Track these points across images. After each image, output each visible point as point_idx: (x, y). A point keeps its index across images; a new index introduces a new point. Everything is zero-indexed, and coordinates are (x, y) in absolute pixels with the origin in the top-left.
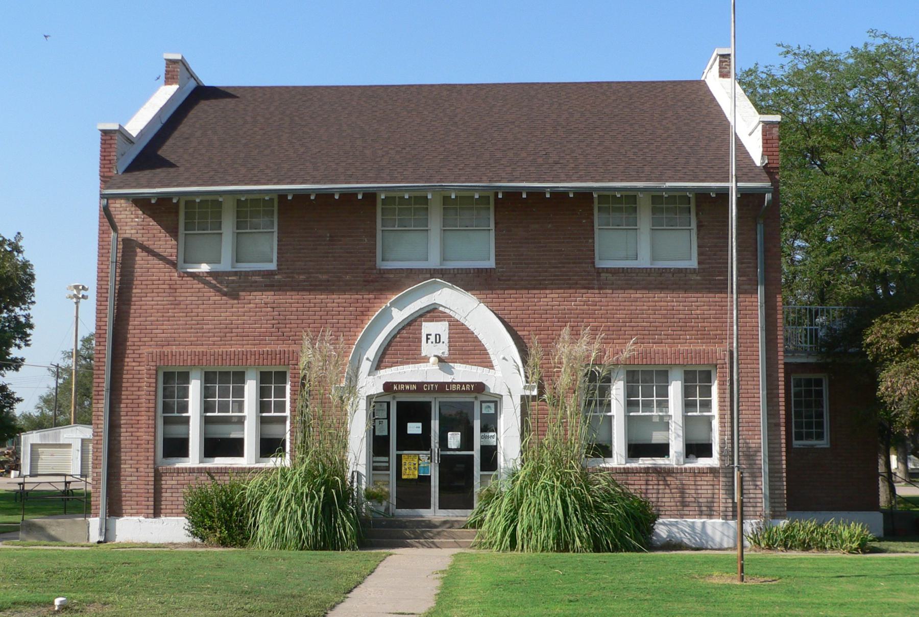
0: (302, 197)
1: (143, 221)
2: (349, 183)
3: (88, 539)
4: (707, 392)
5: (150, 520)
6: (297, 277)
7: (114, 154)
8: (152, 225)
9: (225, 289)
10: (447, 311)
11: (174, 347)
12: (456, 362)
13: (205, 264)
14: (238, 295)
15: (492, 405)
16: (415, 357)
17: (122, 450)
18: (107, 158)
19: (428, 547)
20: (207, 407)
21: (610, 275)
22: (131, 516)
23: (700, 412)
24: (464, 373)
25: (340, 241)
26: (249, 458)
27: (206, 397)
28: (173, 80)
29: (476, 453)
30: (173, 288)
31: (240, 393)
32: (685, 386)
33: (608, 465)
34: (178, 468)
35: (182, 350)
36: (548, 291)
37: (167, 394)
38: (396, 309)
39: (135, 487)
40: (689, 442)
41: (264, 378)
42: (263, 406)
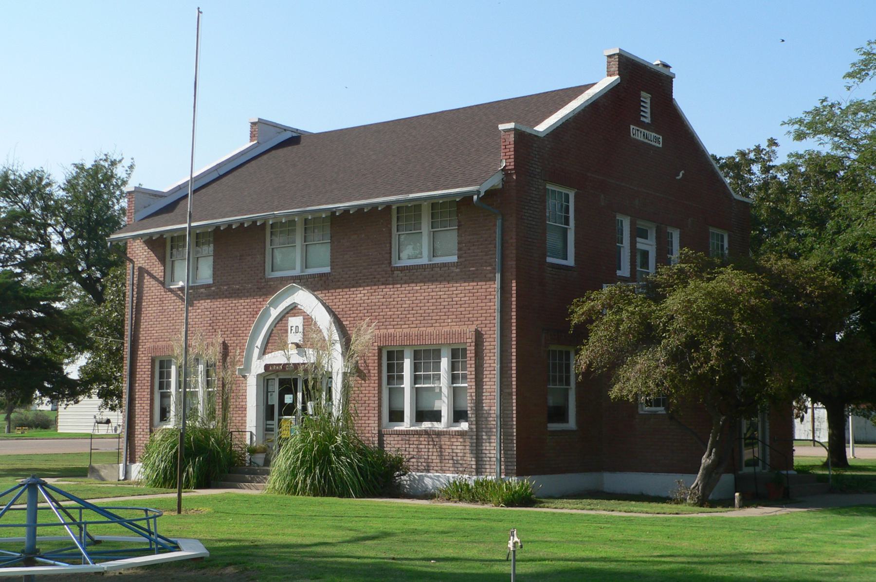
2: (216, 218)
14: (193, 303)
16: (283, 346)
21: (399, 272)
27: (415, 371)
34: (397, 430)
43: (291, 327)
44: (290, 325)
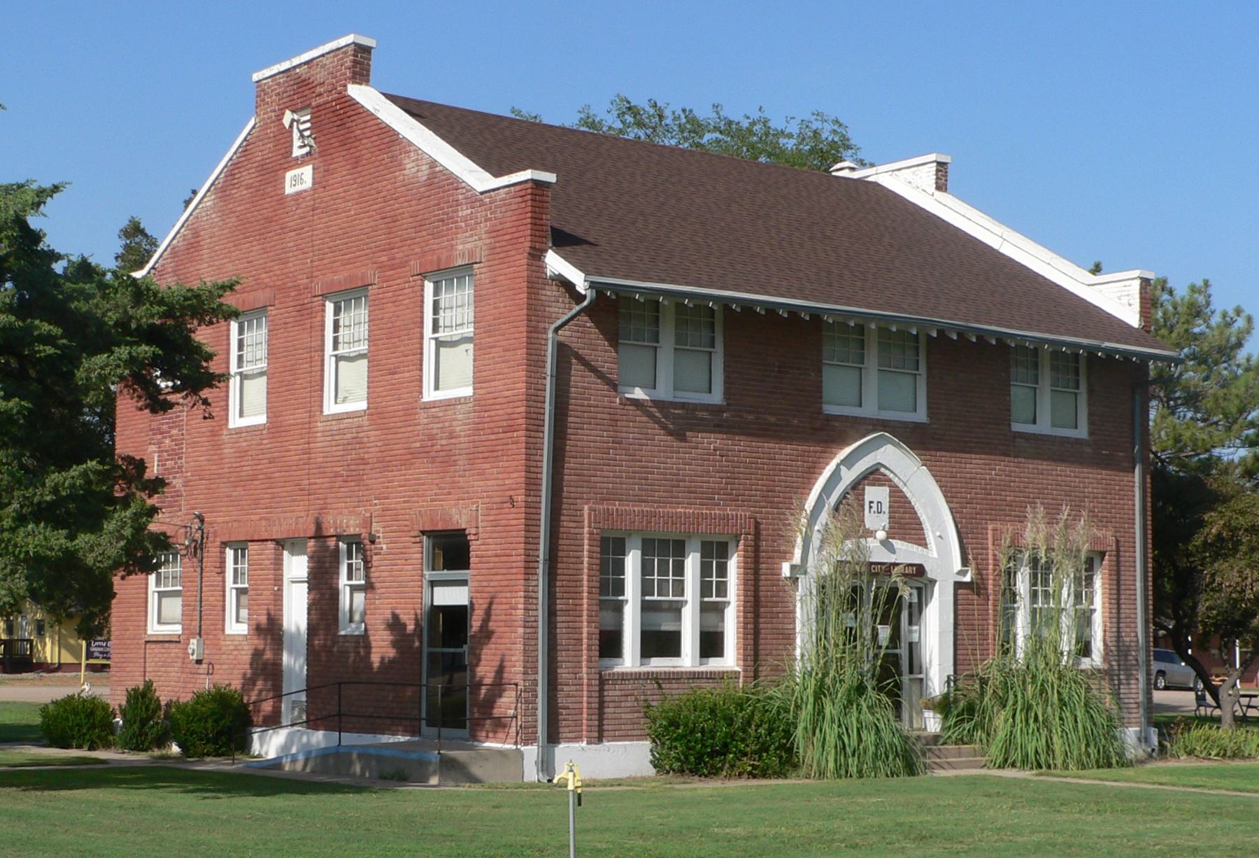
0: (748, 306)
7: (549, 217)
10: (887, 472)
12: (894, 538)
14: (685, 435)
17: (559, 648)
20: (646, 588)
24: (905, 553)
33: (618, 669)
36: (973, 456)
40: (706, 630)
42: (705, 589)
43: (871, 502)
44: (867, 499)
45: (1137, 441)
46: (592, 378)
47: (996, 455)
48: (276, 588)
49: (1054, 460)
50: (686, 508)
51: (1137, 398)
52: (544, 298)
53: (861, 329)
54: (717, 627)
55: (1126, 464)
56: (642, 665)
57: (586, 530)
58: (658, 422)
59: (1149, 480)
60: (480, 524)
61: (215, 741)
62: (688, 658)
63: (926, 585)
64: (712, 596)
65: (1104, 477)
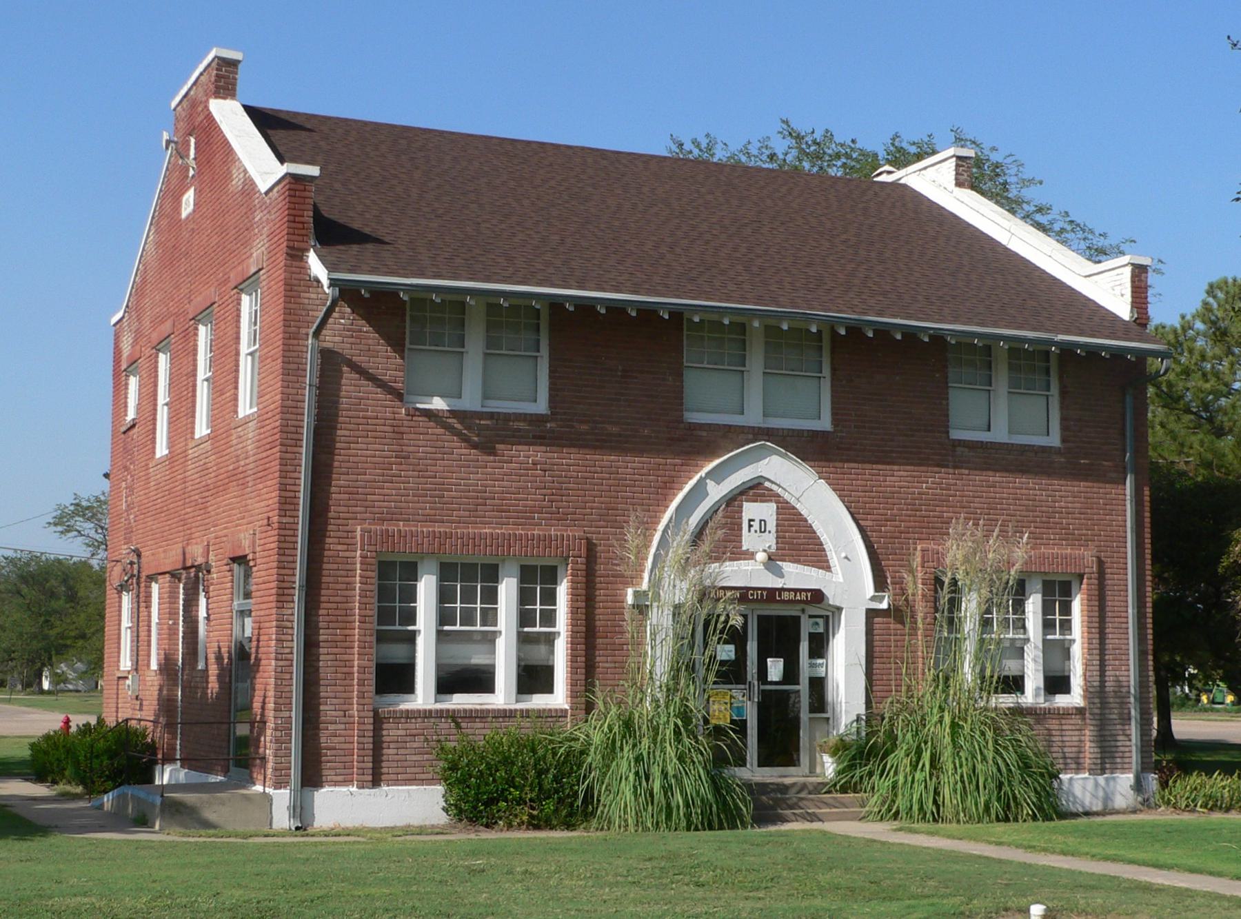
0: (586, 308)
1: (352, 324)
2: (604, 290)
3: (271, 824)
4: (550, 597)
5: (367, 791)
6: (641, 431)
8: (366, 332)
9: (476, 439)
10: (774, 487)
11: (401, 523)
12: (784, 561)
13: (438, 398)
14: (494, 448)
15: (821, 621)
17: (322, 682)
18: (297, 219)
19: (808, 821)
20: (444, 617)
21: (966, 450)
22: (335, 786)
23: (1060, 634)
24: (797, 576)
25: (636, 378)
26: (502, 696)
28: (227, 92)
29: (803, 687)
30: (399, 434)
31: (491, 596)
32: (521, 588)
33: (404, 706)
35: (413, 529)
36: (896, 467)
37: (384, 593)
38: (713, 482)
39: (342, 739)
41: (527, 575)
42: (525, 618)
43: (750, 520)
45: (1128, 448)
46: (368, 386)
47: (929, 466)
48: (171, 622)
49: (1007, 471)
50: (494, 528)
51: (1129, 399)
52: (306, 301)
53: (988, 350)
54: (548, 660)
55: (1114, 475)
56: (436, 701)
57: (359, 552)
58: (458, 433)
59: (1147, 492)
60: (258, 549)
61: (109, 778)
62: (502, 696)
63: (833, 613)
64: (476, 626)
65: (1082, 489)
